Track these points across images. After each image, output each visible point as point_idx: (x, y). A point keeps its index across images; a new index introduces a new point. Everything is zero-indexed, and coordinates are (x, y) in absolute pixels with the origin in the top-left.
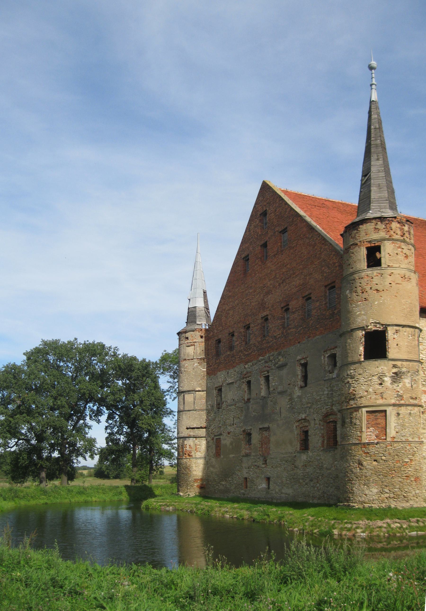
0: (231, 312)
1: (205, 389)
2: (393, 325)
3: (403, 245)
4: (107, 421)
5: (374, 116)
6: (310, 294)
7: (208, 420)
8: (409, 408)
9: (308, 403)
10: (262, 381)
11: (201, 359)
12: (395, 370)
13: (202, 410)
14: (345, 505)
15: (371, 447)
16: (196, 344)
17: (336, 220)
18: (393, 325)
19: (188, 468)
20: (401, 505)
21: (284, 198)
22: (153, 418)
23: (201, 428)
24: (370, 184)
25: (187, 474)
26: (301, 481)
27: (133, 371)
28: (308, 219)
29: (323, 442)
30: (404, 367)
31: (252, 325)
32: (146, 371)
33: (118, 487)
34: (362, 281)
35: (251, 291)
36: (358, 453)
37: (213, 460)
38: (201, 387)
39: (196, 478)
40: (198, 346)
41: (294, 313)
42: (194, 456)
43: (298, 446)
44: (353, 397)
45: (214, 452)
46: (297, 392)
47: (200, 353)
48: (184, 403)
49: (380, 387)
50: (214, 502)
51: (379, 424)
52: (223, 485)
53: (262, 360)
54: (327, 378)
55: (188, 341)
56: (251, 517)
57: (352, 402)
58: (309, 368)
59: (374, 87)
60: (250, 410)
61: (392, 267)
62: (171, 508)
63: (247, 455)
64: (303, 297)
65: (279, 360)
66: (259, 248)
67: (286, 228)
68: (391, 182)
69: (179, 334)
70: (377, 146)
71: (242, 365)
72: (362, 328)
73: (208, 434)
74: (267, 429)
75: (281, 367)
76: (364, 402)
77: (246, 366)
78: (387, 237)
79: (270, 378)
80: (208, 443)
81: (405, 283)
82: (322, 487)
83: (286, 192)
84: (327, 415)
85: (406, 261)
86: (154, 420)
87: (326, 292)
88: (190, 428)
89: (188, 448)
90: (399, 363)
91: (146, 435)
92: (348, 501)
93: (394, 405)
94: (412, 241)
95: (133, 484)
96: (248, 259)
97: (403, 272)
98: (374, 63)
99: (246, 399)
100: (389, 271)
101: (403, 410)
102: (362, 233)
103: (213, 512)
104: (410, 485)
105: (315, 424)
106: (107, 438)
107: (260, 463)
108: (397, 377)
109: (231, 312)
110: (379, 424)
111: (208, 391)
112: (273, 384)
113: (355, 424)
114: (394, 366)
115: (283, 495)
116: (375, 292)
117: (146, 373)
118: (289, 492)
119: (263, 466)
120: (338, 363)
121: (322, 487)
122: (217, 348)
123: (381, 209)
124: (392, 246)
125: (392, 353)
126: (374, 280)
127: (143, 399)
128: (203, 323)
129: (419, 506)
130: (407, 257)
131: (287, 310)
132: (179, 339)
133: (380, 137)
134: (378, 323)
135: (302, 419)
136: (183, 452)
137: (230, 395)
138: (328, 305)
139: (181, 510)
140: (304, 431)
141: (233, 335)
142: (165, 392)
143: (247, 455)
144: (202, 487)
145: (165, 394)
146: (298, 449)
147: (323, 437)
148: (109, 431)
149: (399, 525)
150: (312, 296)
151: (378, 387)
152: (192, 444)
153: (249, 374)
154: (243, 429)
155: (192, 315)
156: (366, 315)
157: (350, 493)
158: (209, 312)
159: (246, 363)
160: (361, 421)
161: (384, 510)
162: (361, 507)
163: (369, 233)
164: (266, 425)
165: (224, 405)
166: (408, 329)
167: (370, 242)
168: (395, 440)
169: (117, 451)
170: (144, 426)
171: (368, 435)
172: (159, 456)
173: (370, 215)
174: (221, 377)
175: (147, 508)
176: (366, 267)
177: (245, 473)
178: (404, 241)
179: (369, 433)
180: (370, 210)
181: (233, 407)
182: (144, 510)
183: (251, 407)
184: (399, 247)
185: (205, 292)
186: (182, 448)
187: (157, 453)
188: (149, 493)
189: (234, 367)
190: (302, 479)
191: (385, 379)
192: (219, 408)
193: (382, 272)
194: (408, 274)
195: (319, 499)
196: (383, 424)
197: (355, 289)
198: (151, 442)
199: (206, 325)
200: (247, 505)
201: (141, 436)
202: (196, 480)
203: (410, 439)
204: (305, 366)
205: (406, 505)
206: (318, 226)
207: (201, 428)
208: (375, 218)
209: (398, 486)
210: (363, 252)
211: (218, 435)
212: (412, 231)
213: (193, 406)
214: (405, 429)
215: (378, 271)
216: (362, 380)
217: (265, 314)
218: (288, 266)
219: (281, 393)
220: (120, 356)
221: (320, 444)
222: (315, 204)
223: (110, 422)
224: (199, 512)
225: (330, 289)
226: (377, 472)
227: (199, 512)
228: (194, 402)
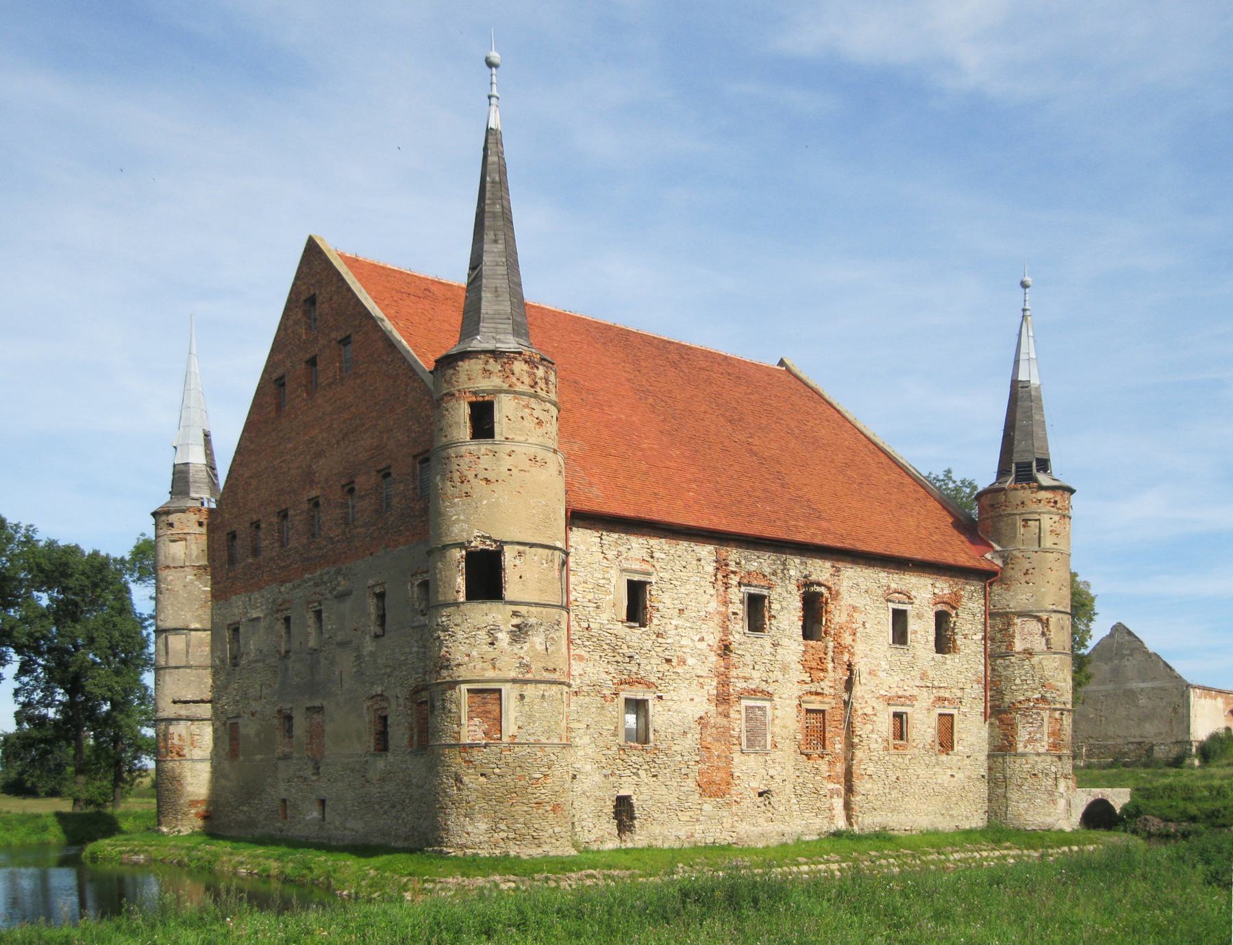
0: (254, 482)
1: (209, 626)
2: (512, 543)
3: (533, 403)
4: (17, 678)
5: (492, 159)
6: (389, 467)
7: (215, 688)
8: (542, 686)
9: (386, 667)
10: (311, 620)
11: (199, 567)
12: (516, 621)
13: (204, 667)
14: (435, 851)
15: (475, 752)
16: (188, 537)
17: (446, 326)
18: (512, 543)
19: (176, 779)
20: (528, 852)
21: (345, 276)
22: (117, 672)
23: (202, 701)
24: (480, 286)
25: (175, 791)
26: (376, 807)
27: (71, 575)
28: (388, 325)
29: (411, 738)
30: (533, 616)
31: (291, 512)
32: (99, 577)
33: (38, 816)
34: (461, 462)
35: (289, 446)
36: (455, 761)
37: (226, 764)
38: (201, 622)
39: (192, 798)
41: (362, 498)
42: (188, 756)
43: (372, 745)
44: (444, 664)
45: (228, 748)
46: (369, 646)
47: (197, 556)
48: (167, 653)
50: (229, 844)
51: (490, 712)
52: (245, 813)
53: (310, 579)
54: (416, 624)
55: (174, 531)
56: (282, 872)
57: (444, 673)
58: (388, 601)
59: (494, 100)
61: (513, 440)
62: (142, 857)
63: (286, 757)
64: (378, 472)
66: (303, 365)
67: (349, 337)
68: (520, 285)
69: (154, 514)
70: (494, 215)
72: (461, 546)
73: (216, 718)
74: (319, 710)
75: (342, 596)
76: (463, 673)
77: (283, 589)
78: (505, 386)
79: (324, 615)
80: (215, 731)
81: (535, 470)
82: (410, 817)
83: (353, 263)
84: (416, 691)
85: (540, 431)
86: (118, 679)
87: (415, 468)
88: (180, 702)
89: (176, 741)
90: (523, 610)
91: (106, 707)
92: (440, 844)
93: (514, 681)
94: (553, 397)
95: (78, 810)
96: (283, 385)
97: (532, 451)
98: (495, 56)
99: (283, 651)
100: (508, 447)
101: (529, 690)
102: (463, 377)
103: (218, 863)
104: (545, 818)
105: (399, 705)
106: (17, 714)
107: (309, 772)
108: (520, 632)
109: (254, 482)
110: (490, 712)
111: (215, 630)
112: (328, 626)
113: (450, 711)
114: (515, 614)
115: (347, 832)
116: (484, 483)
117: (102, 580)
118: (356, 827)
119: (314, 778)
120: (429, 598)
121: (410, 817)
122: (230, 548)
123: (497, 333)
124: (514, 403)
125: (509, 594)
126: (481, 461)
127: (95, 635)
128: (203, 496)
129: (560, 853)
130: (540, 423)
131: (351, 491)
132: (156, 525)
133: (502, 198)
134: (489, 538)
135: (377, 695)
136: (166, 747)
137: (253, 644)
138: (418, 491)
139: (161, 860)
140: (380, 717)
141: (258, 527)
142: (146, 619)
143: (286, 757)
144: (206, 817)
145: (147, 623)
146: (372, 749)
147: (412, 729)
148: (21, 699)
149: (513, 885)
150: (392, 471)
151: (487, 648)
152: (184, 733)
153: (287, 605)
154: (277, 708)
155: (181, 479)
156: (470, 521)
157: (444, 830)
158: (216, 476)
159: (283, 582)
160: (458, 705)
161: (497, 859)
162: (460, 854)
163: (475, 378)
164: (317, 703)
165: (243, 662)
166: (540, 550)
167: (475, 393)
168: (517, 741)
169: (41, 741)
170: (97, 691)
171: (471, 730)
172: (137, 751)
173: (478, 343)
174: (239, 607)
175: (94, 858)
176: (468, 439)
177: (282, 791)
178: (535, 396)
179: (472, 728)
180: (478, 334)
181: (260, 664)
182: (88, 862)
184: (527, 406)
185: (207, 435)
186: (166, 740)
187: (130, 745)
188: (109, 827)
189: (261, 588)
190: (379, 803)
191: (500, 635)
192: (235, 665)
193: (495, 448)
194: (541, 454)
195: (406, 839)
196: (496, 713)
197: (449, 475)
198: (115, 722)
199: (209, 500)
200: (282, 850)
201: (94, 709)
202: (193, 803)
203: (544, 740)
204: (381, 596)
205: (536, 852)
206: (404, 343)
207: (202, 701)
208: (484, 352)
209: (522, 820)
210: (463, 411)
212: (552, 378)
214: (534, 722)
215: (489, 447)
216: (460, 636)
217: (313, 494)
218: (353, 409)
219: (342, 644)
220: (42, 544)
221: (406, 742)
222: (409, 291)
223: (25, 679)
224: (193, 865)
225: (422, 462)
226: (486, 795)
227: (193, 865)
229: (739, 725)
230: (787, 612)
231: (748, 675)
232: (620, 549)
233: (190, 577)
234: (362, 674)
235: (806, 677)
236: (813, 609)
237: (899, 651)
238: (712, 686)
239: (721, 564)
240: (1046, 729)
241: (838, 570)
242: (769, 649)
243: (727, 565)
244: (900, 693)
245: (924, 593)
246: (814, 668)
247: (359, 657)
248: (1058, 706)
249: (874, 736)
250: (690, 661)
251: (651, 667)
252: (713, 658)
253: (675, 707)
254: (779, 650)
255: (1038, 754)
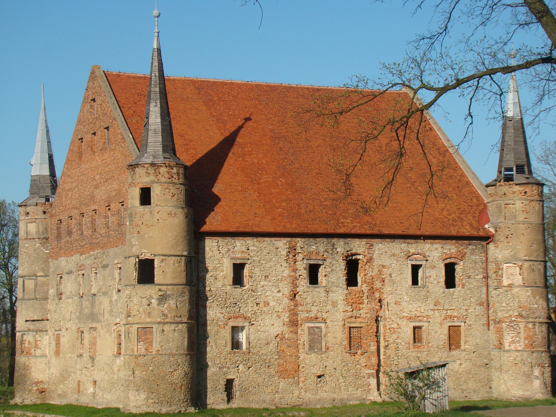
12: (160, 293)
18: (159, 255)
40: (40, 223)
42: (33, 354)
47: (42, 232)
49: (148, 308)
60: (84, 306)
65: (104, 260)
71: (78, 255)
75: (105, 267)
77: (81, 258)
89: (26, 345)
109: (70, 193)
114: (160, 290)
159: (82, 254)
183: (84, 302)
189: (72, 256)
191: (153, 301)
211: (58, 330)
213: (33, 295)
228: (35, 289)
229: (304, 337)
230: (333, 273)
231: (309, 309)
232: (230, 247)
233: (38, 245)
234: (112, 311)
235: (349, 308)
236: (352, 267)
237: (416, 289)
238: (286, 317)
239: (292, 250)
240: (522, 335)
241: (372, 245)
242: (323, 294)
243: (295, 250)
244: (418, 315)
245: (435, 253)
246: (354, 303)
247: (111, 301)
248: (530, 320)
249: (399, 341)
250: (272, 304)
251: (248, 309)
252: (286, 301)
253: (262, 329)
254: (331, 294)
255: (518, 351)
